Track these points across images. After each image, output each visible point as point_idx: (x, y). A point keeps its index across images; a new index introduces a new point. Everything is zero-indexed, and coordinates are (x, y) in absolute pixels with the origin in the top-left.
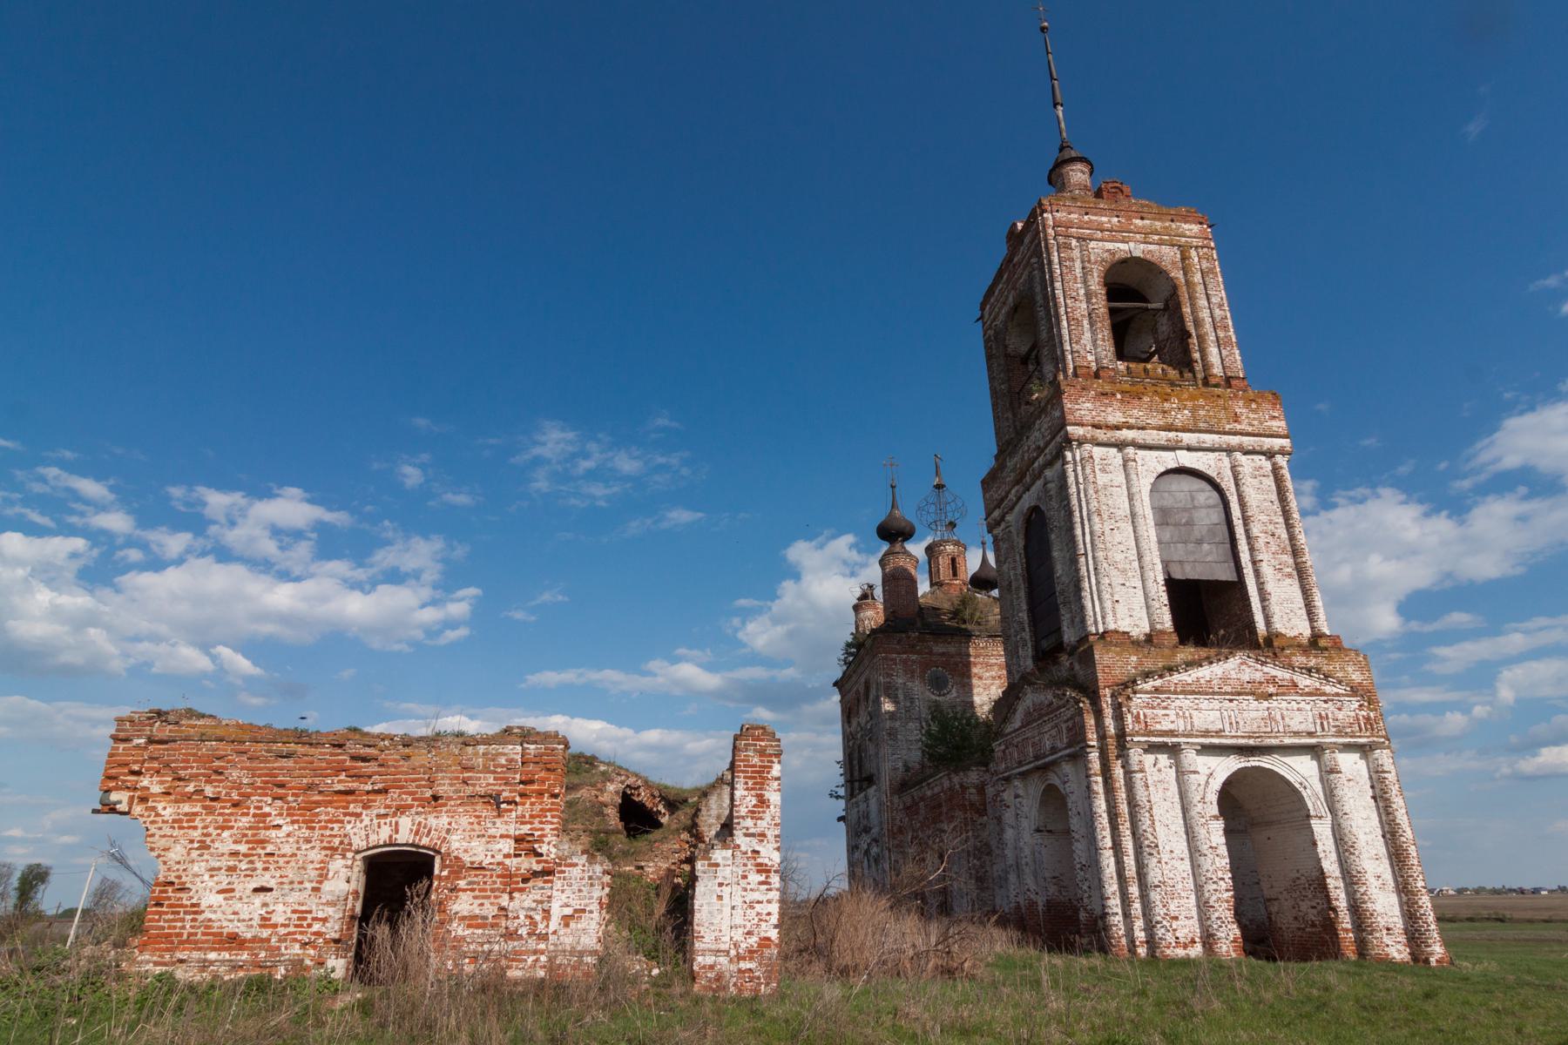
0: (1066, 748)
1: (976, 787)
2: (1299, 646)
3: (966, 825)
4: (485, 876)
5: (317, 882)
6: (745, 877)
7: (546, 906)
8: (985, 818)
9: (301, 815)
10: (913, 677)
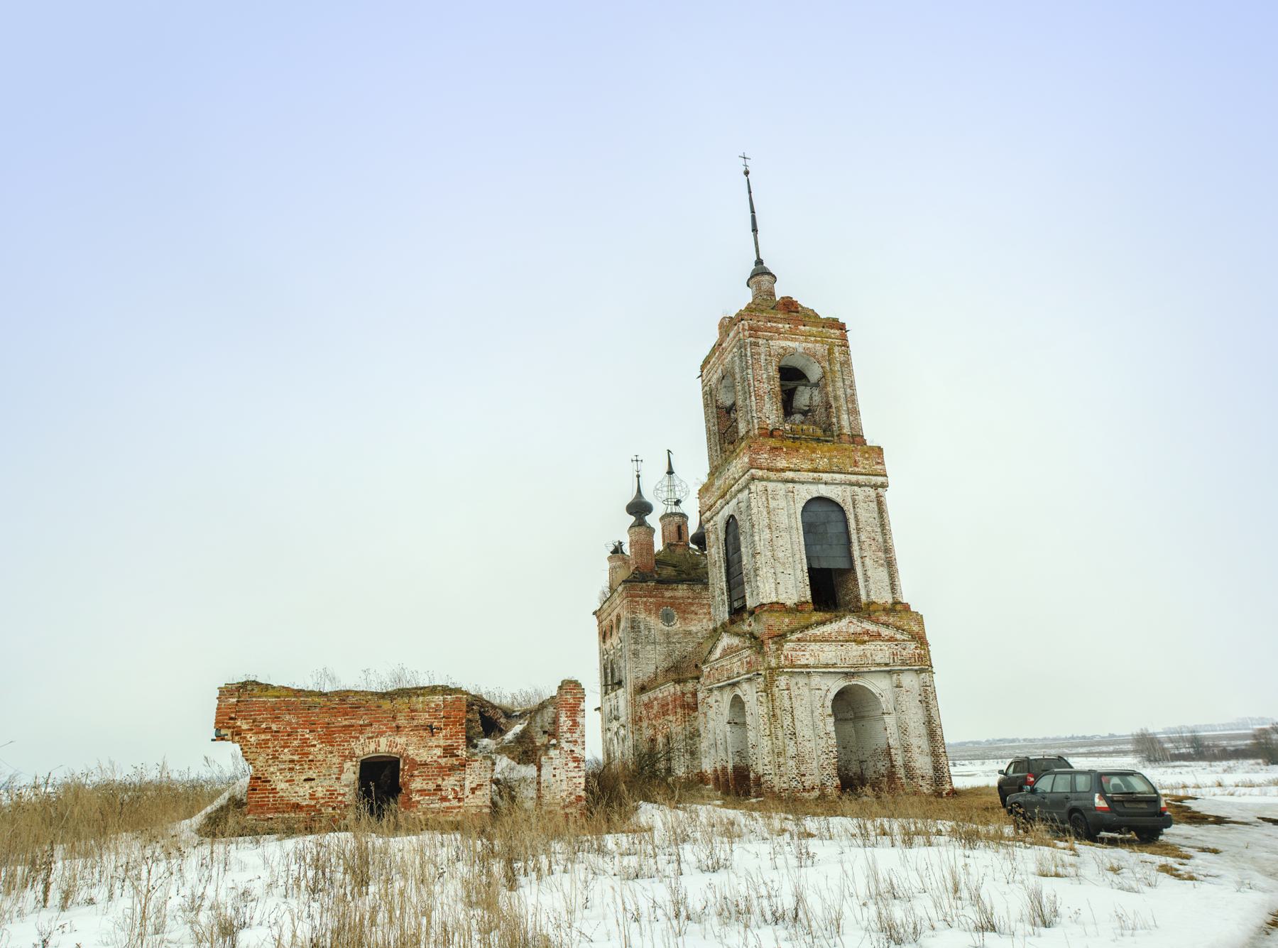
0: (745, 674)
1: (692, 693)
2: (884, 610)
3: (685, 718)
4: (428, 768)
5: (338, 774)
6: (567, 764)
7: (462, 783)
8: (697, 713)
9: (326, 738)
10: (650, 613)
